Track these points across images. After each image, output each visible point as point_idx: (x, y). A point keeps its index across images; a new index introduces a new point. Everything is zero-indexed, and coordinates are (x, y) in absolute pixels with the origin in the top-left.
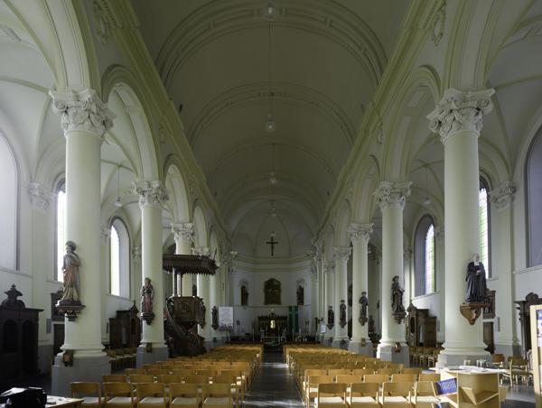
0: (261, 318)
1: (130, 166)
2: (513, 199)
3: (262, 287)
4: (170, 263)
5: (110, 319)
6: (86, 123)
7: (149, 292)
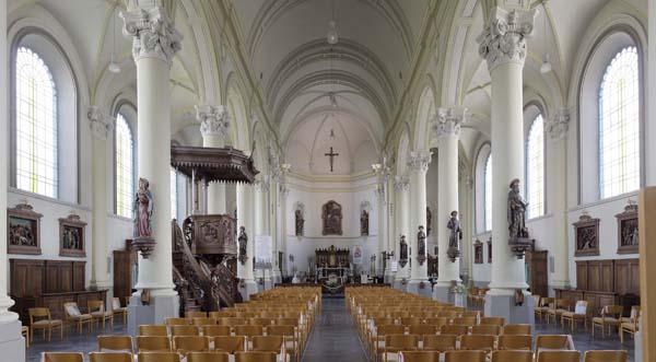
0: (319, 252)
1: (192, 87)
2: (567, 129)
3: (320, 212)
4: (187, 161)
5: (115, 252)
6: (157, 48)
7: (146, 203)
